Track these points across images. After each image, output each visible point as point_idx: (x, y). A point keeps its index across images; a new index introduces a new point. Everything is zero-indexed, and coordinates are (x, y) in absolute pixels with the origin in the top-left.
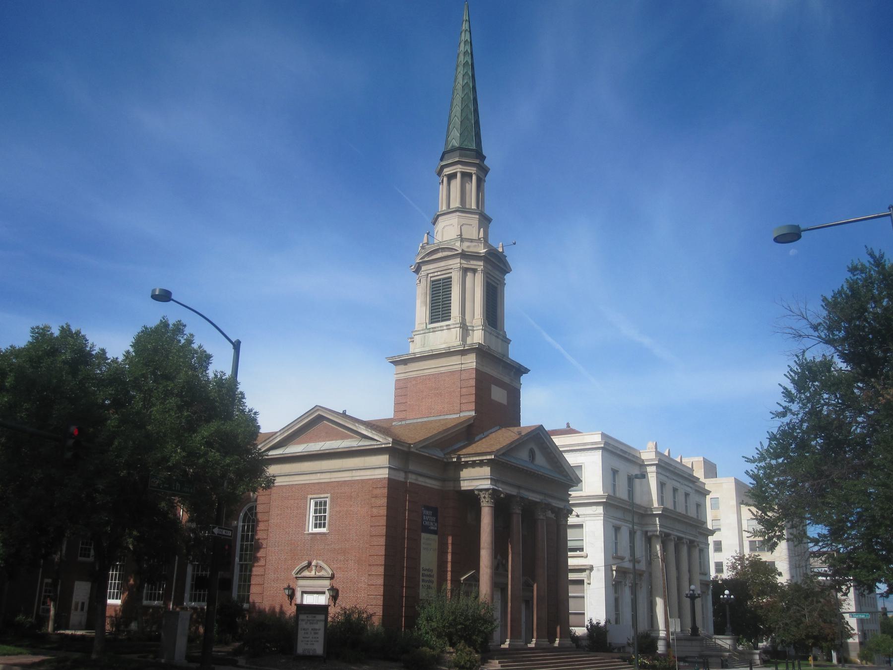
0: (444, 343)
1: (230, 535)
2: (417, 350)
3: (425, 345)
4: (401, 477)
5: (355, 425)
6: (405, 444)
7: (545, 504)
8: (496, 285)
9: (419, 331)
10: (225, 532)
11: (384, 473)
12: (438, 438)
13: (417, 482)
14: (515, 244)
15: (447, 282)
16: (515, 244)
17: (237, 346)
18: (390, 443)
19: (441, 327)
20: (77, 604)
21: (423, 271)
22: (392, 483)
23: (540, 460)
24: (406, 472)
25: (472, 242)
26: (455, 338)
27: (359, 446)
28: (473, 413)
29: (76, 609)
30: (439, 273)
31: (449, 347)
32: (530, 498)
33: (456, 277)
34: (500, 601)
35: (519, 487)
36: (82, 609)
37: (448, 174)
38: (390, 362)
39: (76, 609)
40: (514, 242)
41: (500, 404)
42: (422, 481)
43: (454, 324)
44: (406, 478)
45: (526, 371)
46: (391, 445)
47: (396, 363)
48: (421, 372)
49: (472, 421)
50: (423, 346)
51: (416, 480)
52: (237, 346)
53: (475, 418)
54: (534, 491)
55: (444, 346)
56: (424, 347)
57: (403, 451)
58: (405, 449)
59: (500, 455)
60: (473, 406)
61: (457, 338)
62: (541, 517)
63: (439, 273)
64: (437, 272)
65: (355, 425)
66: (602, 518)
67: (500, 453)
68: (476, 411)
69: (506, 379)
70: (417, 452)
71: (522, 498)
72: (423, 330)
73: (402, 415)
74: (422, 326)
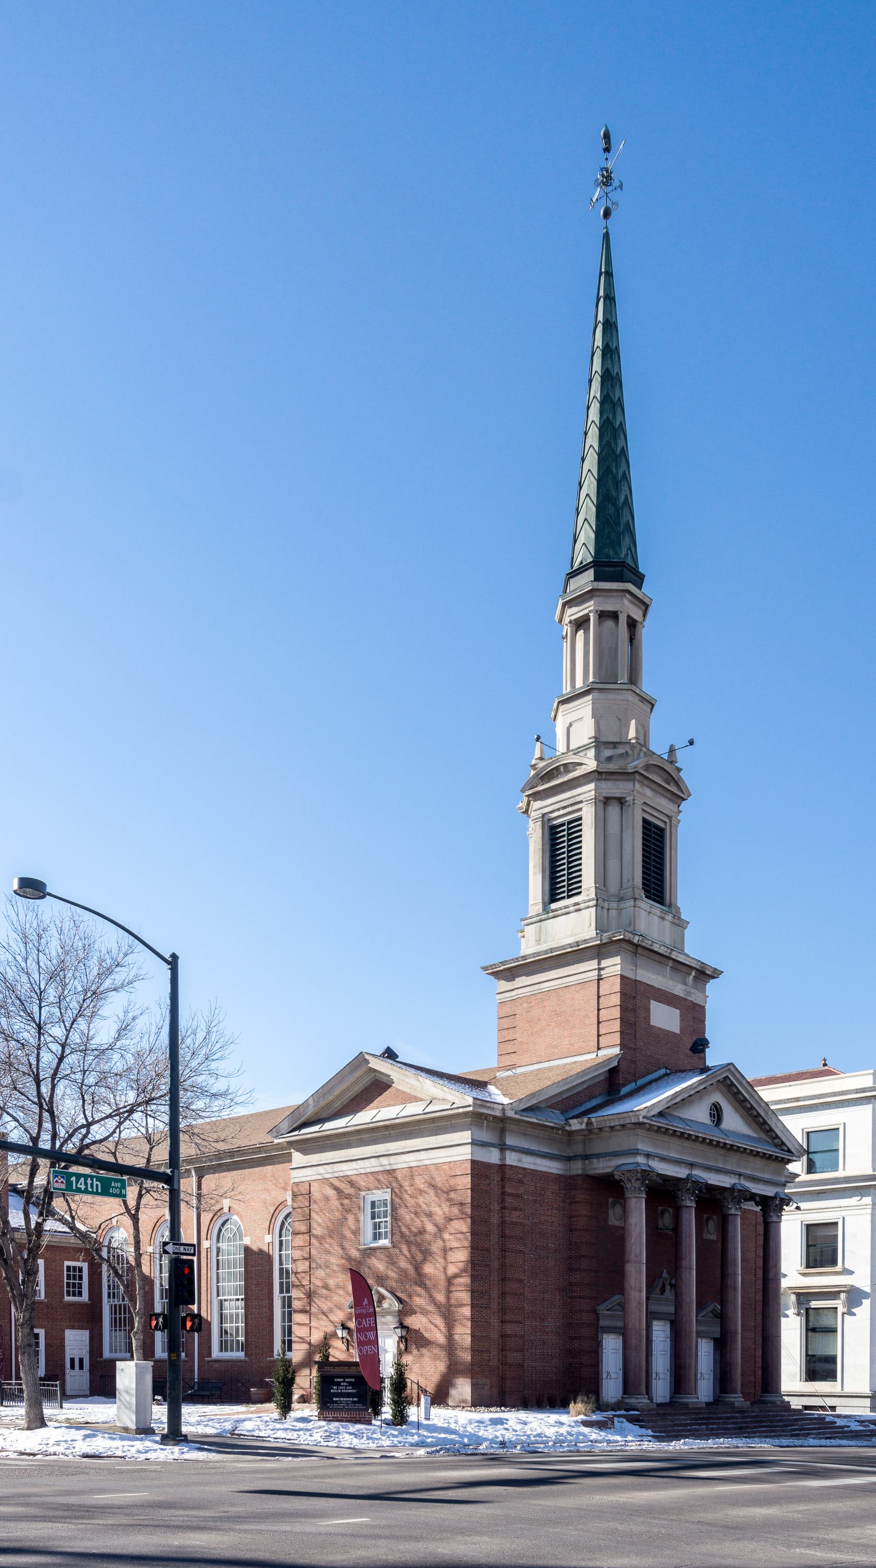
0: (571, 936)
1: (192, 1252)
2: (529, 951)
3: (542, 940)
4: (492, 1157)
5: (419, 1080)
6: (496, 1106)
7: (740, 1190)
8: (661, 825)
9: (531, 917)
10: (185, 1249)
11: (466, 1153)
12: (566, 1096)
13: (519, 1165)
14: (691, 743)
15: (575, 825)
16: (691, 743)
17: (173, 962)
18: (469, 1106)
19: (566, 907)
20: (72, 1360)
21: (535, 810)
22: (478, 1169)
23: (733, 1121)
24: (503, 1148)
25: (615, 747)
26: (588, 925)
27: (425, 1114)
28: (617, 1051)
29: (72, 1367)
30: (562, 812)
31: (577, 942)
32: (710, 1182)
33: (588, 814)
34: (669, 1339)
35: (692, 1165)
36: (81, 1367)
37: (575, 620)
38: (492, 974)
39: (72, 1367)
40: (536, 737)
41: (668, 1034)
42: (529, 1162)
43: (585, 902)
44: (503, 1158)
45: (715, 974)
46: (471, 1109)
47: (498, 975)
48: (536, 987)
49: (615, 1064)
50: (538, 941)
51: (520, 1161)
52: (173, 962)
53: (622, 1059)
54: (718, 1171)
55: (571, 940)
56: (539, 944)
57: (495, 1117)
58: (498, 1114)
59: (654, 1116)
60: (617, 1039)
61: (590, 925)
62: (733, 1211)
63: (562, 812)
64: (558, 810)
65: (419, 1080)
66: (869, 1211)
67: (652, 1113)
68: (622, 1046)
69: (678, 989)
70: (517, 1116)
71: (696, 1183)
72: (538, 915)
73: (508, 1061)
74: (537, 907)
